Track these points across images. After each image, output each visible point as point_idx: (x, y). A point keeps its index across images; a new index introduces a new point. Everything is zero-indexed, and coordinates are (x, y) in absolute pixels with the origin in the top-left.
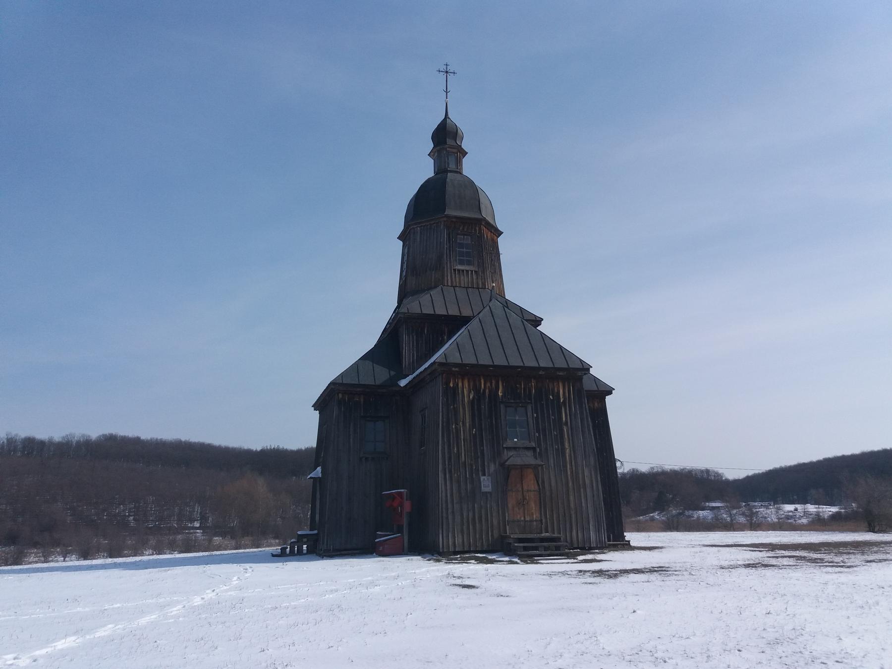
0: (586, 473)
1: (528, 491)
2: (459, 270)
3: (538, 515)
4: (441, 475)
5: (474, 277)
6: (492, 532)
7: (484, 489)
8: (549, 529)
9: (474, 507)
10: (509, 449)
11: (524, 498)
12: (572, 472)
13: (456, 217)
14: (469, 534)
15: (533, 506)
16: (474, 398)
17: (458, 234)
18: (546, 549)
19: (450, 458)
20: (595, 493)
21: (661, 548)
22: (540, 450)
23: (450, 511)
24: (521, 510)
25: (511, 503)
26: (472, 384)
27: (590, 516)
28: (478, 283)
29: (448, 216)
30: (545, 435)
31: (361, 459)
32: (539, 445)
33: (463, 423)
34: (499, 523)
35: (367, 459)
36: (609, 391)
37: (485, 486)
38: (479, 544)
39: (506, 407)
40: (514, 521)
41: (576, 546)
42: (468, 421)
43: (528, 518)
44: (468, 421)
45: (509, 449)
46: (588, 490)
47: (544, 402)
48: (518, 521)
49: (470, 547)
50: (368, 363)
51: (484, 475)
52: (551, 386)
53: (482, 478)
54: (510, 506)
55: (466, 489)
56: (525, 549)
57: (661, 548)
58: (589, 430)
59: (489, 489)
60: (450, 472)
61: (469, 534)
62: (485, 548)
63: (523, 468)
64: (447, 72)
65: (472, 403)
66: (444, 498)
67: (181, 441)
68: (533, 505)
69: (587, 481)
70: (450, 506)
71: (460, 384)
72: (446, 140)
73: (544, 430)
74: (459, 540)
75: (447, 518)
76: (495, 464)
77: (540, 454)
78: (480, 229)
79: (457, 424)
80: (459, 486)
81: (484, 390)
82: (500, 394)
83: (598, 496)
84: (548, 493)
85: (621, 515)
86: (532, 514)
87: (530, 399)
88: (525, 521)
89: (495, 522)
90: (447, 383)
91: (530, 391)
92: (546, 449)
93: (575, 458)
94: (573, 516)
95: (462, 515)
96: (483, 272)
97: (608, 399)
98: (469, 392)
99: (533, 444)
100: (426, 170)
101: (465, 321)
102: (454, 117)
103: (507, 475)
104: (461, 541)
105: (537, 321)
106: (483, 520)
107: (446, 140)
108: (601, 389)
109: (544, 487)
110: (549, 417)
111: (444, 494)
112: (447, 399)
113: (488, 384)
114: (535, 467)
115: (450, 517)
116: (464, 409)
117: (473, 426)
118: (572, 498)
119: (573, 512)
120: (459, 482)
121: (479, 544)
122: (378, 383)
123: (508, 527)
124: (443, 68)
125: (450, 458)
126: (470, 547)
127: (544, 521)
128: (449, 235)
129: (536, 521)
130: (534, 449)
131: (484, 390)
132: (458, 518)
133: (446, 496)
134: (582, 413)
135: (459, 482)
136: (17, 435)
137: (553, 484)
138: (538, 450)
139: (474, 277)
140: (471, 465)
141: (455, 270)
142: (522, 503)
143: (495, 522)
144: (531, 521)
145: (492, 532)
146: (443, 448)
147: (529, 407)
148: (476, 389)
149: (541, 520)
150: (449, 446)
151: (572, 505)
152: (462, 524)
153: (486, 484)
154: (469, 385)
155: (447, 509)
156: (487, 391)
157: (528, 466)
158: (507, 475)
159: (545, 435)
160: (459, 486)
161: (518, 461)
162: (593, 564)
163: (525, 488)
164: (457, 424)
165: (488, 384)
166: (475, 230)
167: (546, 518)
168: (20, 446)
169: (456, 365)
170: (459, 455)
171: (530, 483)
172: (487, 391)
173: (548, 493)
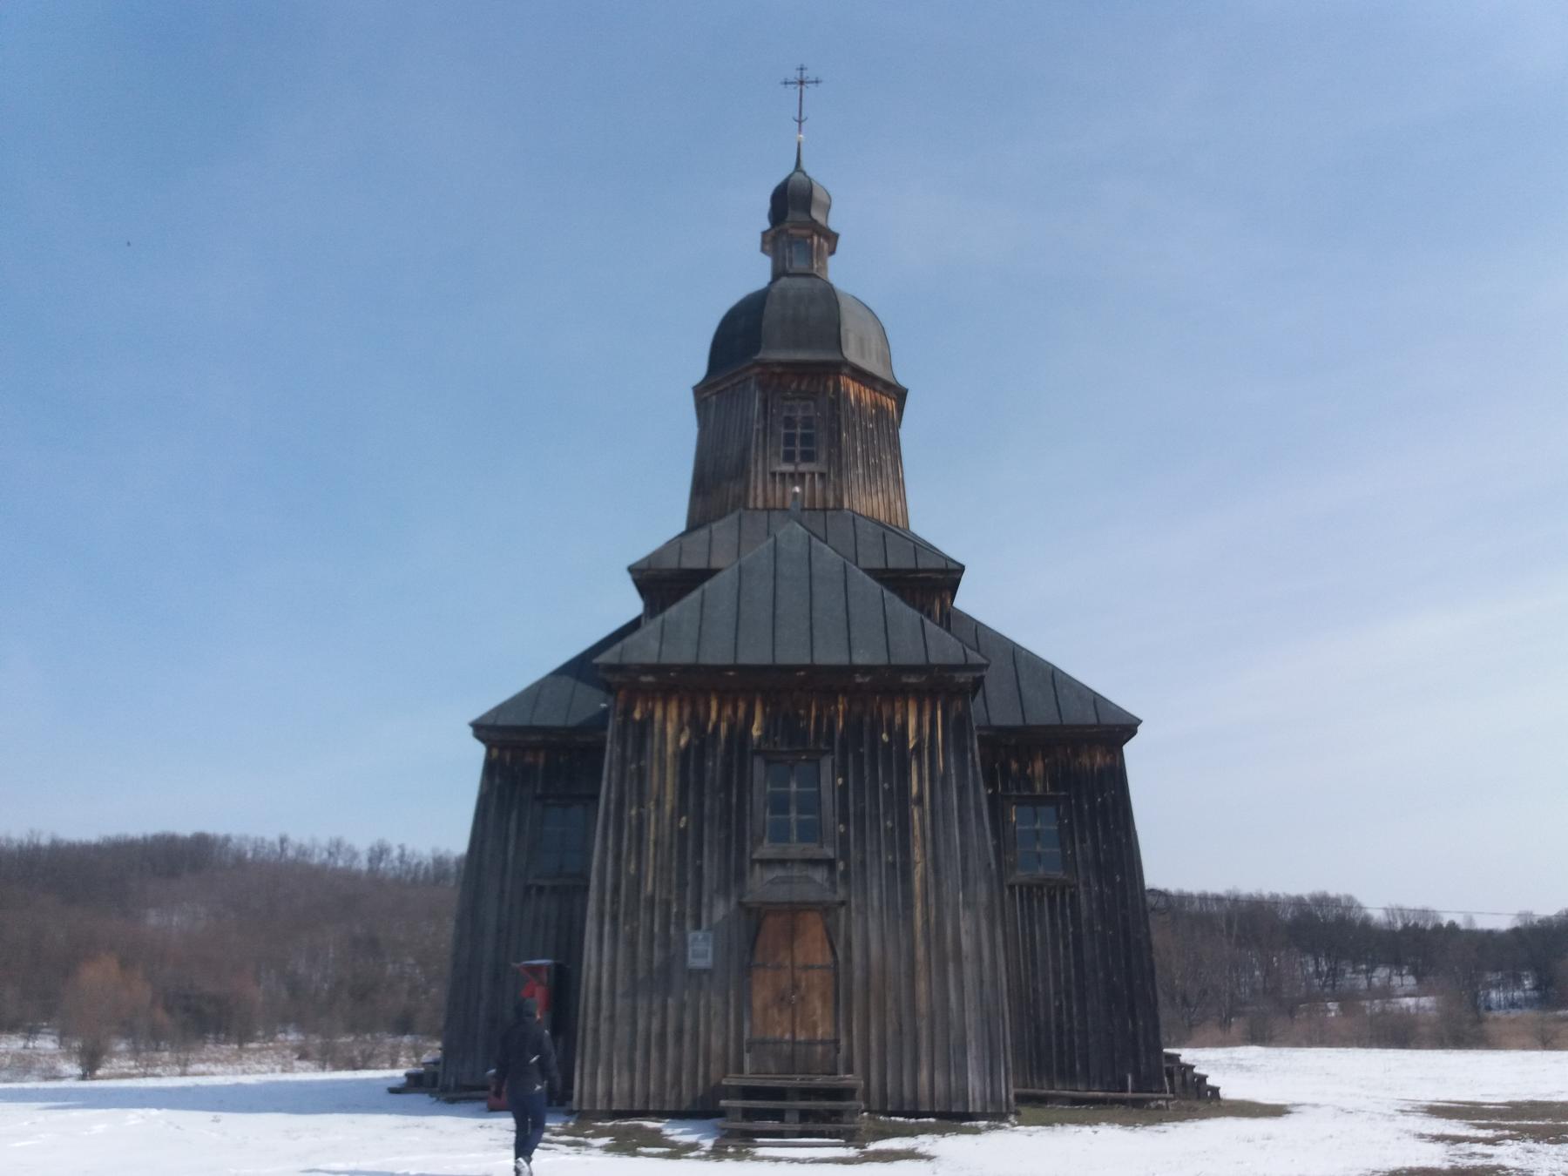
0: (965, 925)
1: (807, 967)
2: (783, 475)
4: (591, 927)
5: (818, 486)
6: (707, 1067)
7: (695, 962)
9: (664, 1007)
11: (795, 987)
12: (926, 922)
13: (780, 364)
14: (646, 1070)
15: (818, 1008)
16: (689, 744)
19: (616, 889)
21: (1277, 1111)
22: (847, 865)
23: (605, 1013)
25: (761, 995)
26: (687, 712)
27: (970, 1035)
28: (825, 500)
29: (765, 365)
30: (861, 831)
31: (527, 889)
32: (845, 855)
34: (726, 1047)
35: (541, 889)
36: (1129, 728)
37: (695, 956)
38: (670, 1096)
40: (764, 1042)
41: (926, 1108)
42: (669, 797)
43: (801, 1037)
44: (669, 797)
45: (767, 863)
46: (969, 970)
47: (865, 750)
49: (647, 1102)
51: (698, 926)
53: (691, 935)
54: (757, 1003)
55: (650, 962)
57: (1277, 1111)
60: (615, 918)
61: (646, 1070)
62: (686, 1105)
63: (795, 910)
64: (802, 83)
65: (683, 756)
66: (592, 984)
67: (37, 849)
68: (818, 1004)
69: (967, 943)
70: (605, 1001)
71: (658, 714)
72: (795, 217)
73: (861, 817)
74: (620, 1084)
75: (596, 1030)
77: (846, 875)
78: (837, 384)
79: (641, 805)
80: (633, 956)
81: (716, 727)
82: (756, 732)
84: (858, 974)
85: (1157, 1027)
86: (815, 1027)
87: (830, 742)
88: (794, 1041)
89: (716, 1044)
90: (628, 712)
92: (863, 863)
93: (938, 884)
95: (634, 1023)
96: (839, 474)
97: (1128, 749)
98: (680, 730)
99: (829, 852)
100: (752, 272)
101: (708, 573)
103: (756, 929)
104: (626, 1086)
105: (949, 576)
107: (795, 217)
108: (1107, 720)
109: (848, 959)
110: (875, 787)
111: (593, 973)
113: (728, 711)
114: (826, 910)
115: (604, 1028)
116: (663, 769)
117: (681, 809)
118: (922, 987)
119: (923, 1025)
120: (632, 943)
121: (670, 1096)
123: (747, 1058)
124: (794, 75)
125: (616, 889)
126: (647, 1102)
127: (843, 1042)
128: (765, 403)
129: (823, 1042)
130: (830, 864)
131: (716, 727)
132: (623, 1031)
133: (599, 978)
134: (962, 774)
135: (632, 943)
136: (336, 847)
138: (841, 866)
139: (818, 486)
140: (668, 904)
141: (773, 474)
143: (716, 1044)
144: (811, 1043)
145: (707, 1067)
146: (603, 864)
147: (826, 764)
148: (697, 724)
149: (837, 1041)
150: (618, 857)
151: (922, 1005)
152: (633, 1047)
153: (701, 951)
154: (680, 715)
155: (598, 1009)
156: (724, 727)
160: (633, 956)
161: (781, 894)
162: (1436, 1132)
163: (800, 960)
165: (728, 711)
166: (826, 387)
167: (849, 1032)
168: (453, 870)
170: (637, 881)
171: (812, 947)
172: (724, 727)
173: (858, 974)
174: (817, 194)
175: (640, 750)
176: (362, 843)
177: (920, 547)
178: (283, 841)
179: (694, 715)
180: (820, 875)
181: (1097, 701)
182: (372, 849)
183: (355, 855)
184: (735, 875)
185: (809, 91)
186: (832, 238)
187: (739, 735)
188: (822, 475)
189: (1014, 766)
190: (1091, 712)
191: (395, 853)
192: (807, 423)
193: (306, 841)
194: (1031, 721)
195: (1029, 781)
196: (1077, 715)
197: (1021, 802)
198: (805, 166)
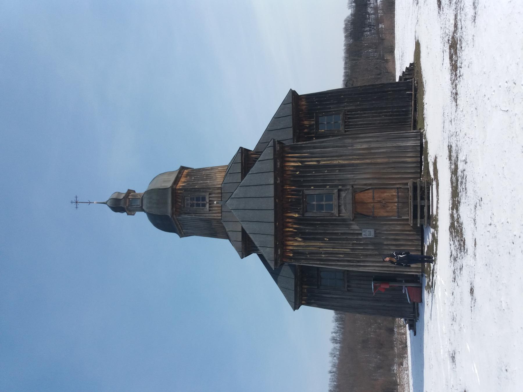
0: (359, 146)
1: (373, 198)
2: (210, 207)
3: (394, 190)
4: (361, 269)
5: (213, 195)
7: (372, 235)
8: (405, 181)
10: (340, 212)
11: (380, 202)
12: (358, 159)
13: (172, 209)
16: (301, 238)
17: (184, 207)
18: (422, 199)
20: (375, 139)
21: (418, 45)
22: (340, 185)
24: (389, 205)
25: (382, 213)
27: (395, 145)
28: (219, 193)
29: (173, 214)
30: (328, 181)
31: (348, 291)
32: (336, 186)
33: (320, 248)
34: (400, 224)
35: (348, 286)
36: (293, 93)
38: (416, 243)
39: (307, 212)
40: (398, 212)
42: (318, 244)
44: (318, 244)
45: (340, 212)
46: (373, 145)
47: (302, 179)
48: (398, 208)
50: (279, 278)
51: (361, 234)
52: (289, 173)
53: (363, 236)
54: (385, 214)
55: (372, 250)
56: (422, 217)
57: (418, 45)
58: (323, 142)
59: (372, 231)
60: (358, 262)
62: (419, 237)
63: (355, 202)
64: (77, 202)
65: (305, 239)
69: (365, 146)
71: (291, 248)
72: (122, 204)
73: (324, 181)
76: (351, 224)
77: (343, 186)
78: (179, 189)
79: (321, 253)
81: (295, 229)
82: (297, 216)
83: (378, 137)
87: (300, 191)
88: (398, 202)
89: (399, 228)
90: (290, 258)
91: (294, 190)
92: (339, 180)
94: (394, 160)
96: (210, 188)
97: (300, 93)
102: (107, 196)
103: (361, 215)
105: (243, 152)
106: (397, 237)
107: (122, 204)
109: (370, 185)
111: (377, 268)
112: (303, 259)
113: (290, 225)
114: (355, 192)
117: (322, 240)
118: (379, 161)
120: (366, 256)
121: (416, 243)
122: (293, 276)
123: (403, 218)
124: (74, 205)
127: (398, 186)
128: (186, 213)
129: (398, 193)
130: (340, 191)
131: (295, 229)
134: (310, 148)
135: (366, 256)
136: (332, 355)
137: (368, 176)
138: (340, 187)
139: (213, 195)
140: (353, 244)
141: (210, 210)
142: (384, 205)
143: (399, 228)
144: (398, 197)
146: (341, 266)
147: (307, 192)
148: (294, 235)
149: (398, 188)
150: (338, 261)
153: (368, 233)
156: (295, 226)
157: (354, 198)
158: (361, 215)
159: (328, 181)
161: (350, 207)
163: (371, 200)
164: (321, 253)
165: (290, 225)
166: (180, 193)
168: (339, 315)
169: (276, 252)
171: (367, 196)
172: (295, 226)
173: (375, 182)
174: (114, 197)
175: (302, 254)
176: (330, 346)
177: (234, 161)
178: (330, 372)
179: (291, 236)
180: (343, 194)
181: (284, 104)
182: (333, 343)
183: (335, 348)
184: (344, 222)
185: (79, 200)
186: (129, 192)
187: (298, 221)
188: (210, 194)
189: (306, 131)
190: (288, 105)
191: (334, 335)
192: (192, 199)
193: (331, 365)
194: (291, 125)
195: (311, 126)
196: (289, 110)
197: (317, 128)
198: (105, 201)
